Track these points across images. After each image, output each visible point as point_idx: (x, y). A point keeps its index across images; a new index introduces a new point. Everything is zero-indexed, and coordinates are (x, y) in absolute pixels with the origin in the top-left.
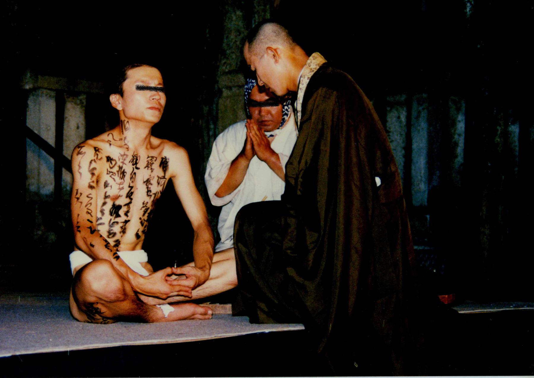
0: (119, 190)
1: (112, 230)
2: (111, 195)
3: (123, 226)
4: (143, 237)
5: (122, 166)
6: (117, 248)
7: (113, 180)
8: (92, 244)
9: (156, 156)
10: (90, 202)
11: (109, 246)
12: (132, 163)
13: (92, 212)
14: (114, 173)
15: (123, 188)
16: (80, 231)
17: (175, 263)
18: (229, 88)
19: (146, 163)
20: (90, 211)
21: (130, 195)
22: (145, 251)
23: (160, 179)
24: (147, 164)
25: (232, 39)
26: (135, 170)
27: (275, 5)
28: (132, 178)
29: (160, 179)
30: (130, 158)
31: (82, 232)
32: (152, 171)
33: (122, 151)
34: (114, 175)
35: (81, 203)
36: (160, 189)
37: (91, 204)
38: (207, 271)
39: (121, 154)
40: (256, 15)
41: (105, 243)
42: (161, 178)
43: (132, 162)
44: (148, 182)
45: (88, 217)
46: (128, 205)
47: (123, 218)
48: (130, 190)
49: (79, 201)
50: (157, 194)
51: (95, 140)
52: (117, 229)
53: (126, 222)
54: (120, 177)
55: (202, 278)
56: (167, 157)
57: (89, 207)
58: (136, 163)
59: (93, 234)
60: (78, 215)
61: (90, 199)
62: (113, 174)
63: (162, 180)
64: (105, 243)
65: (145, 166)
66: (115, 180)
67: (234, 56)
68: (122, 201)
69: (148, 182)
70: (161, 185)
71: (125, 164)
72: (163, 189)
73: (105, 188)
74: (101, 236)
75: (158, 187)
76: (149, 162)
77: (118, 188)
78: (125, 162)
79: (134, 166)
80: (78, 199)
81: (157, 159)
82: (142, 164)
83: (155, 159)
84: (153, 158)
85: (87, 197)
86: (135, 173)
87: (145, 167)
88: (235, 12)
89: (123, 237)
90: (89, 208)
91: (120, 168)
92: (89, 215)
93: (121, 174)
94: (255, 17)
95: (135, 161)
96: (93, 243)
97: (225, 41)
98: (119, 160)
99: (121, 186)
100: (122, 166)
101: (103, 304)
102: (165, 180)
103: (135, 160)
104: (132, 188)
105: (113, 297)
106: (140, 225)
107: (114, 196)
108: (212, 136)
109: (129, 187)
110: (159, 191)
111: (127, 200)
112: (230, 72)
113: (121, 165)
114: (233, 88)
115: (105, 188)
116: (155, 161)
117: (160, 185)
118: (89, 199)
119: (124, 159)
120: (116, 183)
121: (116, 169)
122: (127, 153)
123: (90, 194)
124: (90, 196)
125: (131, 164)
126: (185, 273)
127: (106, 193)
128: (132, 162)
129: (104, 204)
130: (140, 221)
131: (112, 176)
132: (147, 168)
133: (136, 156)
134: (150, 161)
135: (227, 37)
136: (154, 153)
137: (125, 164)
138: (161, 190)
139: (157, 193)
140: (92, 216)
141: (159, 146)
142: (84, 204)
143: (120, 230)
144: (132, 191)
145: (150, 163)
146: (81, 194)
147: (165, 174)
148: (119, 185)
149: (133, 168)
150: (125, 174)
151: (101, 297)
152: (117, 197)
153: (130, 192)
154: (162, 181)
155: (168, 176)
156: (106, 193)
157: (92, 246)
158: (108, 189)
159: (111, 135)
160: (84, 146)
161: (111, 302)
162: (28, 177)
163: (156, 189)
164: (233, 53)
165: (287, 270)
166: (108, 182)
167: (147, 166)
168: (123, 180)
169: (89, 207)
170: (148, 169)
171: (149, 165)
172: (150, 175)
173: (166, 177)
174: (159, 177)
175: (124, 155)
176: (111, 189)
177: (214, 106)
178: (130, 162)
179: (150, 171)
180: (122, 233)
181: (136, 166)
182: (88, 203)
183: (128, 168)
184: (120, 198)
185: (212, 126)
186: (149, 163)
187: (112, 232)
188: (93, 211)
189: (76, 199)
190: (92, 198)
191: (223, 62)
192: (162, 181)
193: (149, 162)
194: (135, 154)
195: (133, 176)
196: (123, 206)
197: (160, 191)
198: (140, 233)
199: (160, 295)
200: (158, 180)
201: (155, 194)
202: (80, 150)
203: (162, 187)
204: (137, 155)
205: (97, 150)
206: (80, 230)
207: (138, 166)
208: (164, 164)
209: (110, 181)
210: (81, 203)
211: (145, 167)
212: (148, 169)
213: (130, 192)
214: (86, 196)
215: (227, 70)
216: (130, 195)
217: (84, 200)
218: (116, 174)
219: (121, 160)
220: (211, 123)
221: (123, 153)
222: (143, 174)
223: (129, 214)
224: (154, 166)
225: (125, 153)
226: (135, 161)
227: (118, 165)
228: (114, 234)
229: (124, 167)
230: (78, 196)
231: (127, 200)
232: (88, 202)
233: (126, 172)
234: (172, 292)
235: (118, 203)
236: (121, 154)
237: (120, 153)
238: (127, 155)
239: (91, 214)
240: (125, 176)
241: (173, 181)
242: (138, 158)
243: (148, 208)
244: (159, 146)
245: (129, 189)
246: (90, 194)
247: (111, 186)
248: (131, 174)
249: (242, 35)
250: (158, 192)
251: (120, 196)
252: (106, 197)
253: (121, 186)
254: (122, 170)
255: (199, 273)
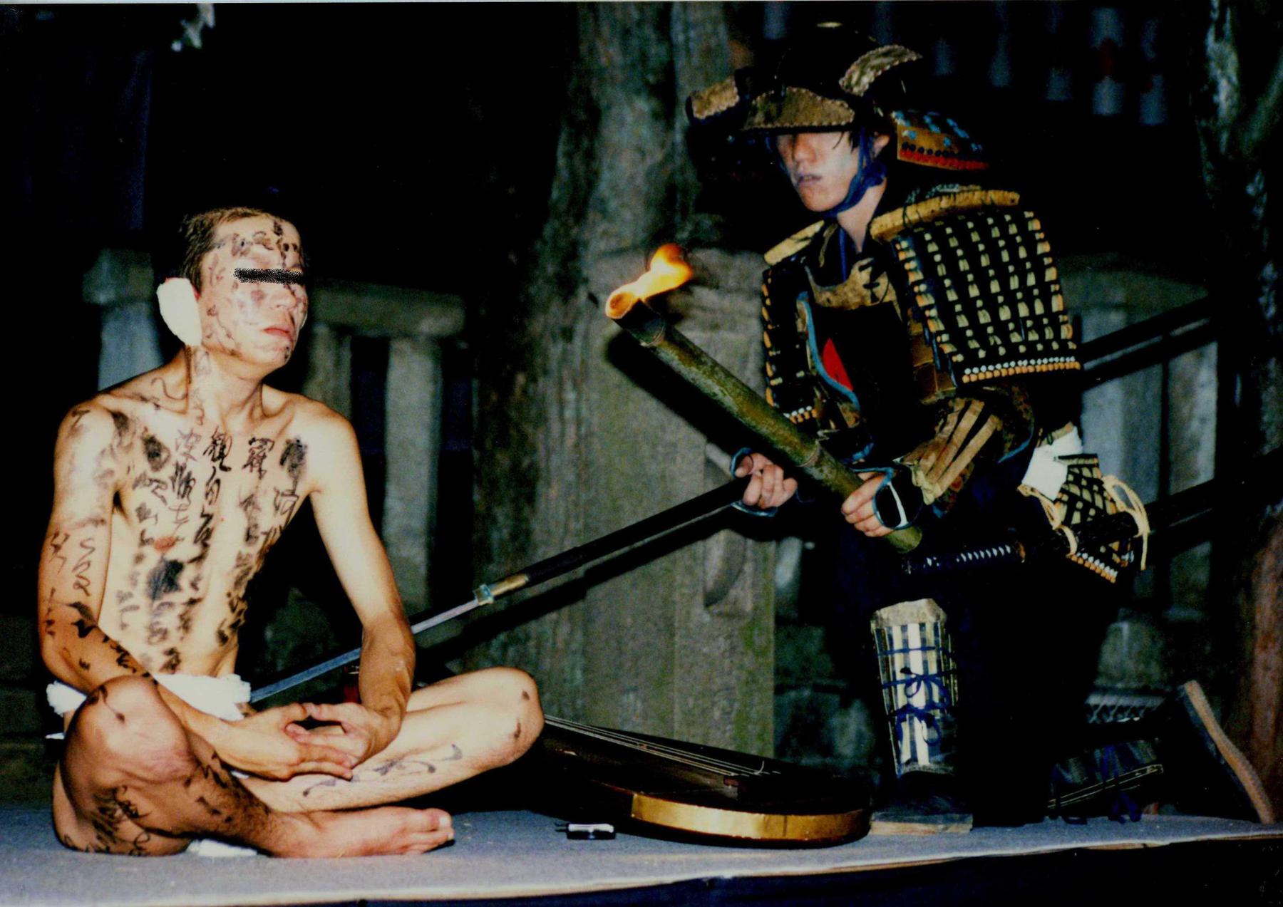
0: (176, 526)
1: (158, 623)
2: (156, 538)
3: (184, 614)
4: (234, 640)
5: (185, 464)
7: (159, 500)
8: (83, 661)
9: (272, 439)
10: (86, 560)
11: (127, 661)
12: (212, 455)
13: (89, 584)
14: (163, 483)
15: (185, 520)
16: (52, 633)
17: (1136, 539)
19: (248, 454)
20: (83, 582)
21: (204, 537)
22: (52, 709)
23: (279, 498)
24: (250, 458)
26: (220, 474)
28: (211, 493)
29: (279, 498)
30: (206, 442)
31: (58, 634)
32: (261, 477)
33: (184, 424)
34: (163, 487)
35: (64, 559)
36: (280, 521)
37: (89, 564)
38: (395, 719)
39: (182, 434)
41: (117, 655)
42: (283, 495)
43: (210, 453)
44: (248, 503)
45: (78, 596)
46: (199, 559)
47: (186, 593)
48: (206, 523)
49: (60, 553)
50: (272, 534)
51: (120, 397)
52: (170, 620)
53: (192, 602)
54: (179, 493)
55: (383, 734)
56: (303, 442)
57: (84, 570)
58: (222, 456)
60: (53, 591)
61: (89, 550)
62: (160, 485)
63: (284, 499)
64: (117, 655)
65: (245, 462)
66: (164, 500)
68: (185, 551)
69: (248, 503)
70: (284, 510)
71: (194, 459)
72: (287, 521)
73: (141, 520)
74: (106, 639)
75: (275, 515)
76: (253, 454)
77: (174, 519)
78: (193, 453)
79: (217, 464)
80: (57, 548)
81: (276, 444)
82: (237, 455)
83: (269, 444)
84: (266, 443)
85: (82, 545)
86: (218, 482)
87: (245, 466)
89: (184, 640)
90: (84, 574)
91: (180, 469)
92: (81, 592)
93: (180, 485)
95: (219, 451)
96: (86, 660)
98: (177, 448)
99: (182, 515)
100: (185, 464)
101: (138, 789)
102: (294, 499)
103: (218, 449)
104: (208, 517)
105: (162, 769)
106: (228, 609)
107: (164, 539)
109: (203, 515)
110: (277, 526)
111: (196, 551)
113: (182, 460)
115: (141, 520)
116: (270, 450)
117: (279, 512)
118: (85, 551)
119: (189, 445)
120: (170, 509)
121: (167, 472)
122: (198, 430)
123: (90, 539)
124: (89, 544)
125: (208, 458)
126: (340, 719)
127: (143, 533)
128: (210, 453)
129: (139, 559)
130: (228, 600)
131: (158, 491)
132: (249, 467)
133: (222, 437)
134: (257, 451)
136: (266, 430)
137: (194, 459)
138: (283, 525)
139: (270, 531)
140: (87, 594)
141: (281, 410)
142: (71, 564)
143: (178, 623)
144: (210, 526)
145: (258, 455)
146: (67, 537)
147: (295, 483)
148: (175, 513)
149: (214, 468)
150: (192, 483)
151: (130, 768)
152: (170, 543)
153: (205, 529)
154: (286, 502)
155: (302, 492)
156: (143, 533)
157: (84, 666)
158: (148, 524)
159: (159, 384)
160: (87, 412)
161: (157, 783)
163: (271, 521)
166: (149, 506)
167: (250, 464)
168: (185, 499)
169: (84, 570)
170: (251, 471)
171: (255, 462)
172: (257, 487)
173: (297, 492)
174: (278, 492)
175: (191, 434)
176: (156, 523)
178: (205, 453)
179: (255, 473)
180: (182, 630)
181: (221, 464)
182: (83, 561)
183: (201, 469)
184: (178, 543)
186: (255, 455)
187: (158, 627)
188: (92, 581)
189: (52, 549)
190: (93, 549)
192: (287, 503)
193: (253, 454)
194: (221, 431)
195: (211, 490)
196: (185, 564)
197: (280, 527)
198: (227, 633)
199: (277, 768)
200: (275, 500)
201: (267, 534)
202: (77, 422)
203: (285, 516)
204: (225, 434)
205: (120, 419)
206: (56, 631)
207: (226, 463)
208: (294, 454)
209: (153, 503)
210: (64, 559)
211: (245, 466)
212: (251, 471)
213: (205, 529)
214: (78, 545)
216: (204, 537)
217: (72, 551)
218: (167, 487)
219: (183, 449)
221: (187, 432)
222: (238, 482)
223: (200, 585)
224: (266, 465)
225: (195, 431)
226: (219, 451)
227: (173, 460)
228: (164, 634)
229: (191, 466)
230: (58, 541)
231: (196, 551)
232: (80, 560)
233: (194, 480)
234: (303, 761)
235: (172, 555)
236: (182, 434)
237: (179, 431)
238: (198, 437)
239: (88, 588)
240: (191, 488)
241: (41, 565)
242: (228, 444)
243: (250, 569)
244: (281, 410)
245: (203, 520)
246: (90, 539)
247: (156, 516)
248: (208, 484)
250: (275, 530)
251: (177, 539)
252: (143, 542)
253: (182, 515)
254: (185, 474)
255: (376, 721)
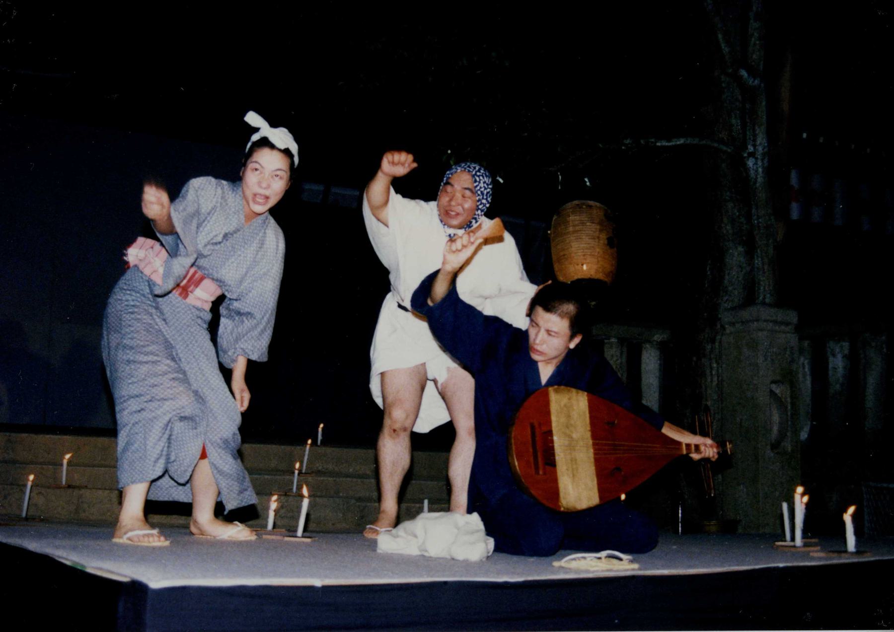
6: (747, 151)
18: (733, 324)
25: (734, 275)
27: (778, 240)
40: (758, 251)
59: (237, 430)
67: (736, 292)
88: (736, 248)
89: (216, 493)
94: (757, 252)
97: (727, 277)
108: (715, 375)
112: (733, 309)
114: (736, 324)
135: (729, 274)
162: (235, 189)
164: (735, 289)
165: (103, 321)
177: (717, 344)
185: (715, 365)
191: (725, 298)
215: (729, 307)
220: (714, 361)
249: (744, 271)
